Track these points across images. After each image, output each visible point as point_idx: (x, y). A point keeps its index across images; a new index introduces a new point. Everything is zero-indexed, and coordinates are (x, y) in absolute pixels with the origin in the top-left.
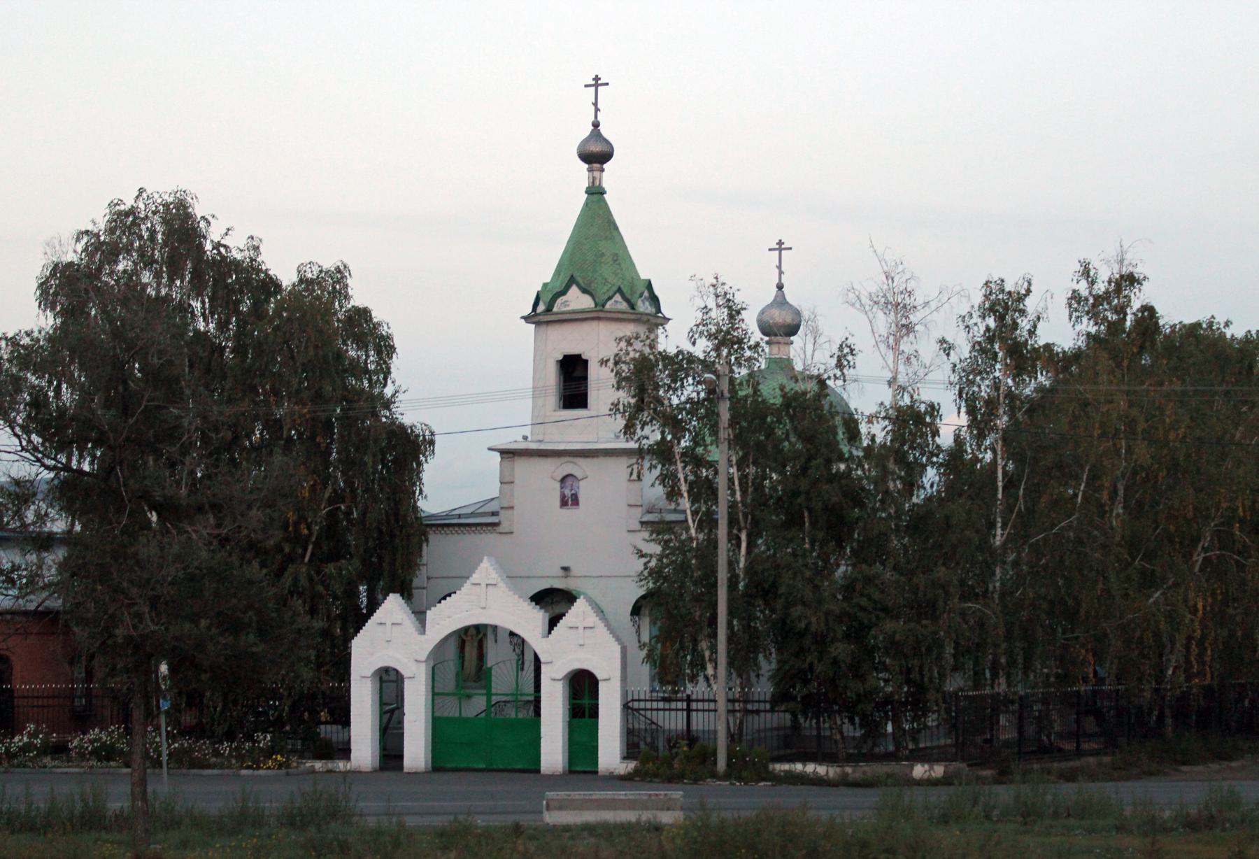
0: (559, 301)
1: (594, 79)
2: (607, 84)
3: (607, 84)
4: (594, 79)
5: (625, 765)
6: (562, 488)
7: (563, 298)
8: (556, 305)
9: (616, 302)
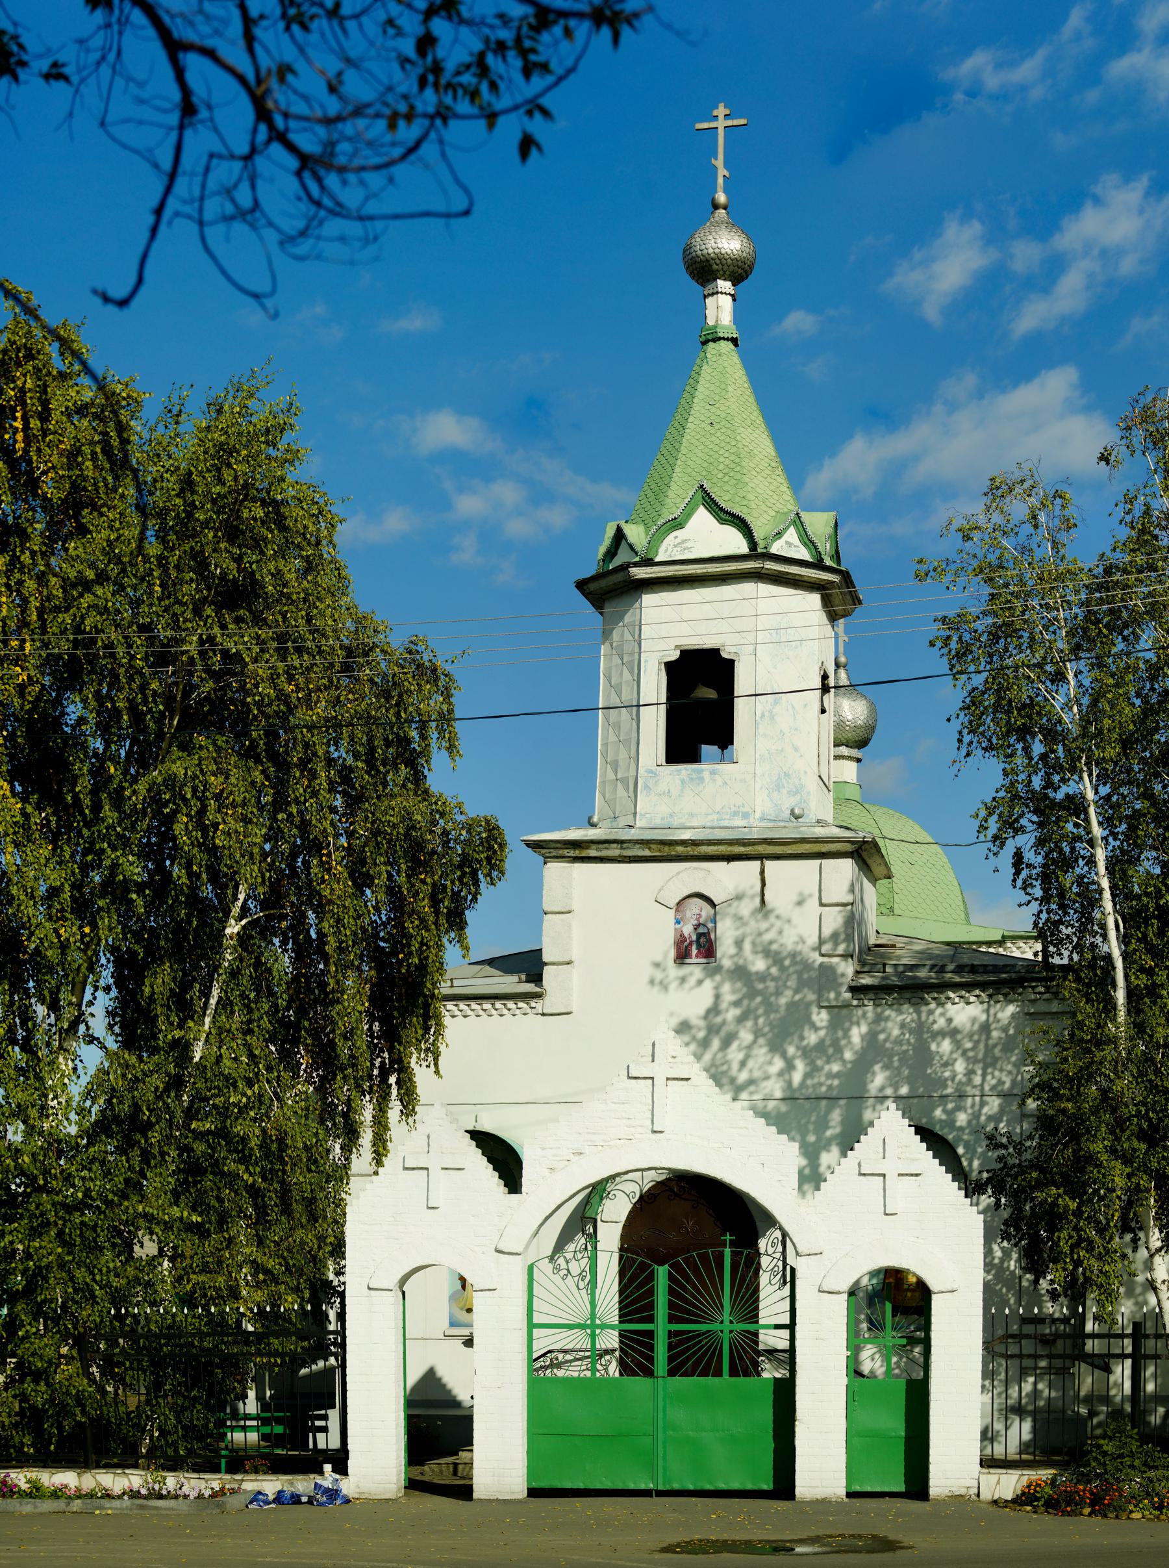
0: (671, 539)
5: (994, 1478)
6: (678, 922)
9: (789, 544)
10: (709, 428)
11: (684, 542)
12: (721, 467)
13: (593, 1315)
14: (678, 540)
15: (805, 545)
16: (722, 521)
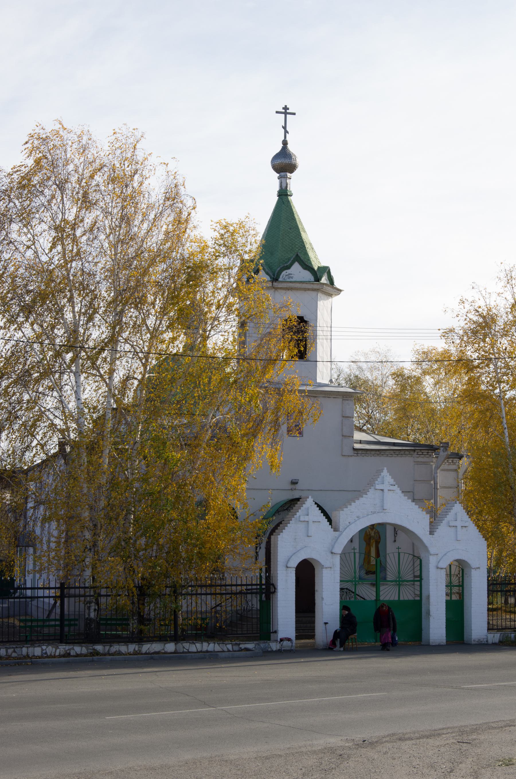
1: (283, 108)
2: (294, 114)
3: (294, 114)
4: (283, 108)
7: (289, 271)
8: (281, 276)
10: (289, 230)
11: (290, 274)
12: (297, 246)
13: (395, 581)
14: (287, 274)
15: (329, 280)
16: (305, 268)
